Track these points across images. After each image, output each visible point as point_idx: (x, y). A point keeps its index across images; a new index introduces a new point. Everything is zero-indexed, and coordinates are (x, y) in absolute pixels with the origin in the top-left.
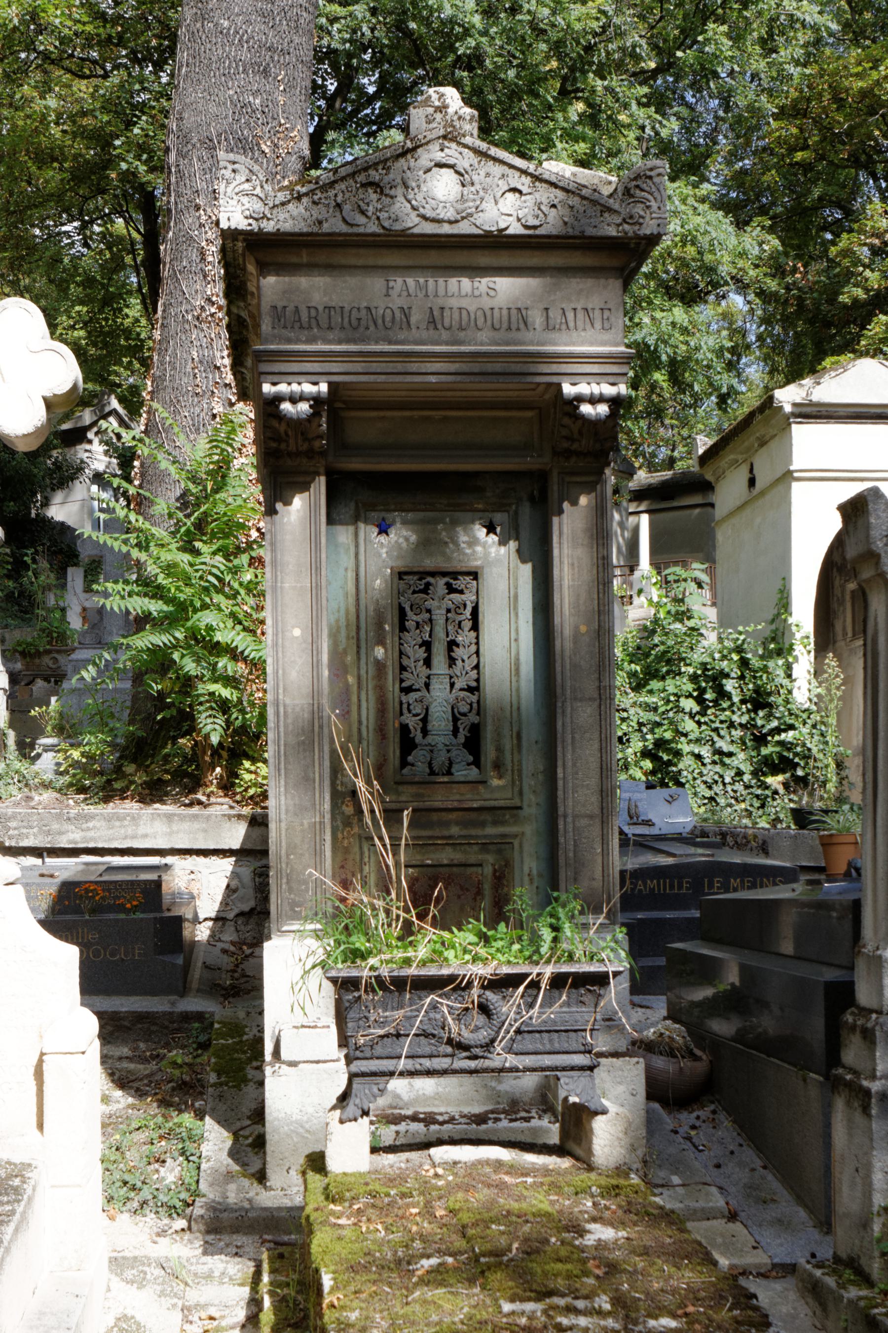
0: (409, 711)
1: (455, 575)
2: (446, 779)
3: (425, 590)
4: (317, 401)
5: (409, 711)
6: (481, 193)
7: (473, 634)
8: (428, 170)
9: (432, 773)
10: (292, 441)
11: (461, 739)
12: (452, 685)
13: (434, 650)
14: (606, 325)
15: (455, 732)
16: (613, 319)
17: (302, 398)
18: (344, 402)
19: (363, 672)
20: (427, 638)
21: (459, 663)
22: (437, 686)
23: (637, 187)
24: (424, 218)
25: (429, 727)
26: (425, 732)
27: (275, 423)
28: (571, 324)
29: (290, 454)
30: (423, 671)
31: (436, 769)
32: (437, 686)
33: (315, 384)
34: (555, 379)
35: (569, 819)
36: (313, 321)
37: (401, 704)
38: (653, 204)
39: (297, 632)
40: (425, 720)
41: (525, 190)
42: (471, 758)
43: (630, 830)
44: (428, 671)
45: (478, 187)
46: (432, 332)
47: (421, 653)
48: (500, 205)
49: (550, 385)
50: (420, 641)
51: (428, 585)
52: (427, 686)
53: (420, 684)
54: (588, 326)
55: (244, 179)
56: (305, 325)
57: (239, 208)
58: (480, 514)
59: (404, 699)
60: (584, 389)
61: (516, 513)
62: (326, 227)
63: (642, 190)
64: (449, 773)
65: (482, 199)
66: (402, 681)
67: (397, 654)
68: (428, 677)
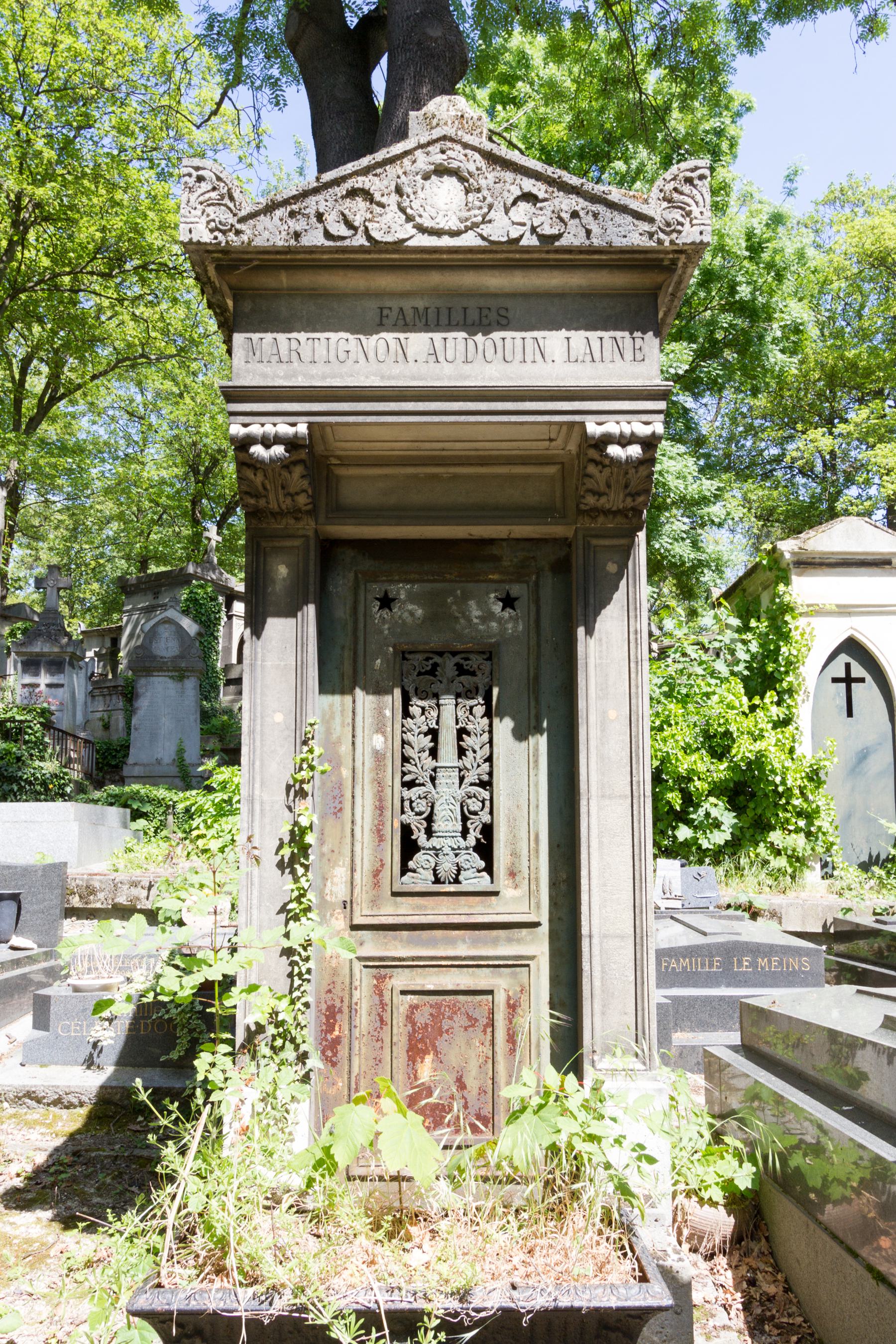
0: (412, 809)
1: (466, 654)
2: (452, 888)
3: (432, 672)
4: (292, 443)
5: (412, 809)
6: (489, 200)
7: (486, 721)
8: (426, 177)
9: (437, 881)
10: (271, 496)
11: (471, 841)
12: (462, 779)
13: (442, 738)
14: (639, 356)
15: (465, 833)
16: (646, 349)
17: (278, 440)
18: (339, 457)
19: (358, 764)
20: (434, 726)
21: (470, 754)
22: (443, 781)
23: (675, 189)
24: (422, 229)
25: (435, 827)
26: (429, 833)
27: (249, 473)
28: (597, 355)
29: (274, 514)
30: (429, 763)
31: (442, 875)
32: (443, 781)
33: (293, 425)
34: (577, 418)
35: (595, 941)
36: (294, 354)
37: (403, 801)
38: (694, 207)
39: (279, 718)
40: (430, 819)
41: (541, 195)
42: (482, 864)
43: (663, 904)
44: (434, 764)
45: (485, 192)
46: (432, 364)
47: (426, 742)
48: (511, 214)
49: (572, 424)
50: (425, 728)
51: (435, 665)
52: (433, 779)
53: (424, 777)
54: (617, 356)
55: (210, 187)
56: (284, 359)
57: (204, 219)
58: (494, 586)
59: (407, 794)
60: (612, 427)
61: (537, 584)
62: (306, 241)
63: (682, 193)
64: (457, 881)
65: (490, 207)
66: (404, 774)
67: (398, 743)
68: (435, 770)
